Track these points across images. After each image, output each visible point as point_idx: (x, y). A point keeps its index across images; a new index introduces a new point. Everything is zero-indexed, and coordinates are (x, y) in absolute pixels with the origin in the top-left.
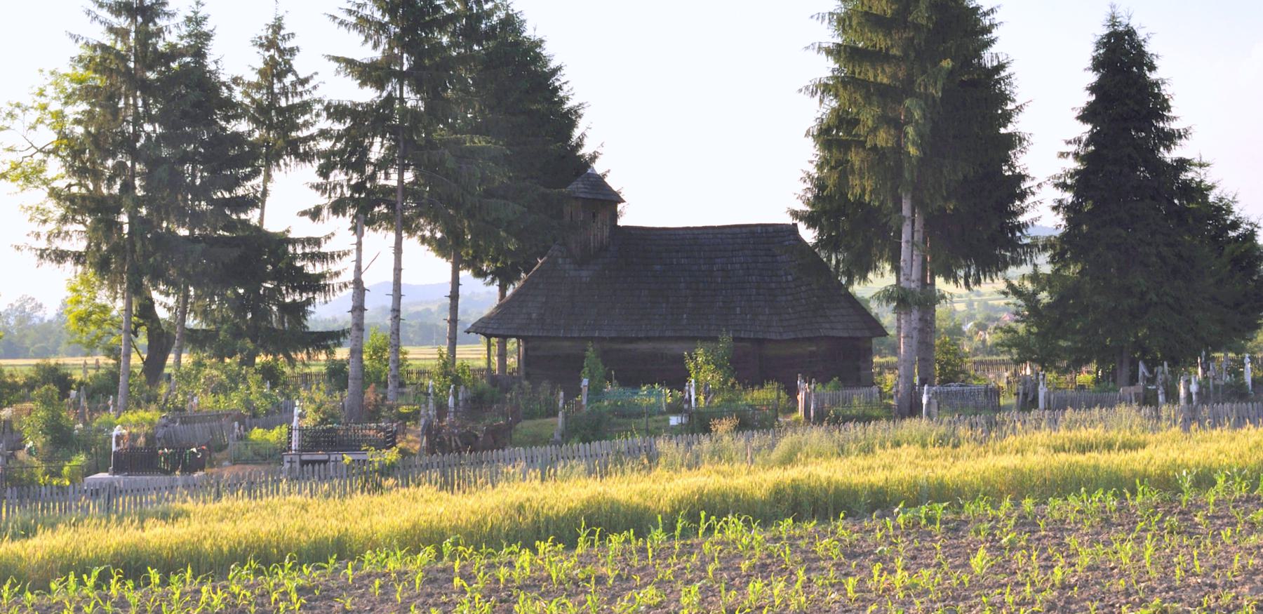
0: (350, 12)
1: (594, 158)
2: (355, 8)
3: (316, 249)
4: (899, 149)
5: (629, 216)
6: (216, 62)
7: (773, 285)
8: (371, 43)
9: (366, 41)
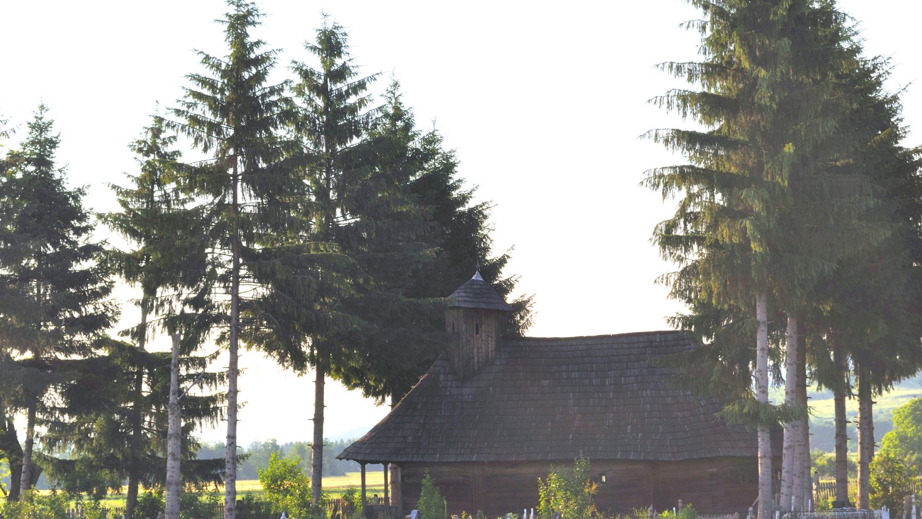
0: (178, 112)
1: (502, 261)
2: (185, 108)
3: (200, 370)
4: (745, 247)
5: (539, 327)
6: (60, 171)
7: (669, 400)
8: (201, 146)
9: (196, 143)
